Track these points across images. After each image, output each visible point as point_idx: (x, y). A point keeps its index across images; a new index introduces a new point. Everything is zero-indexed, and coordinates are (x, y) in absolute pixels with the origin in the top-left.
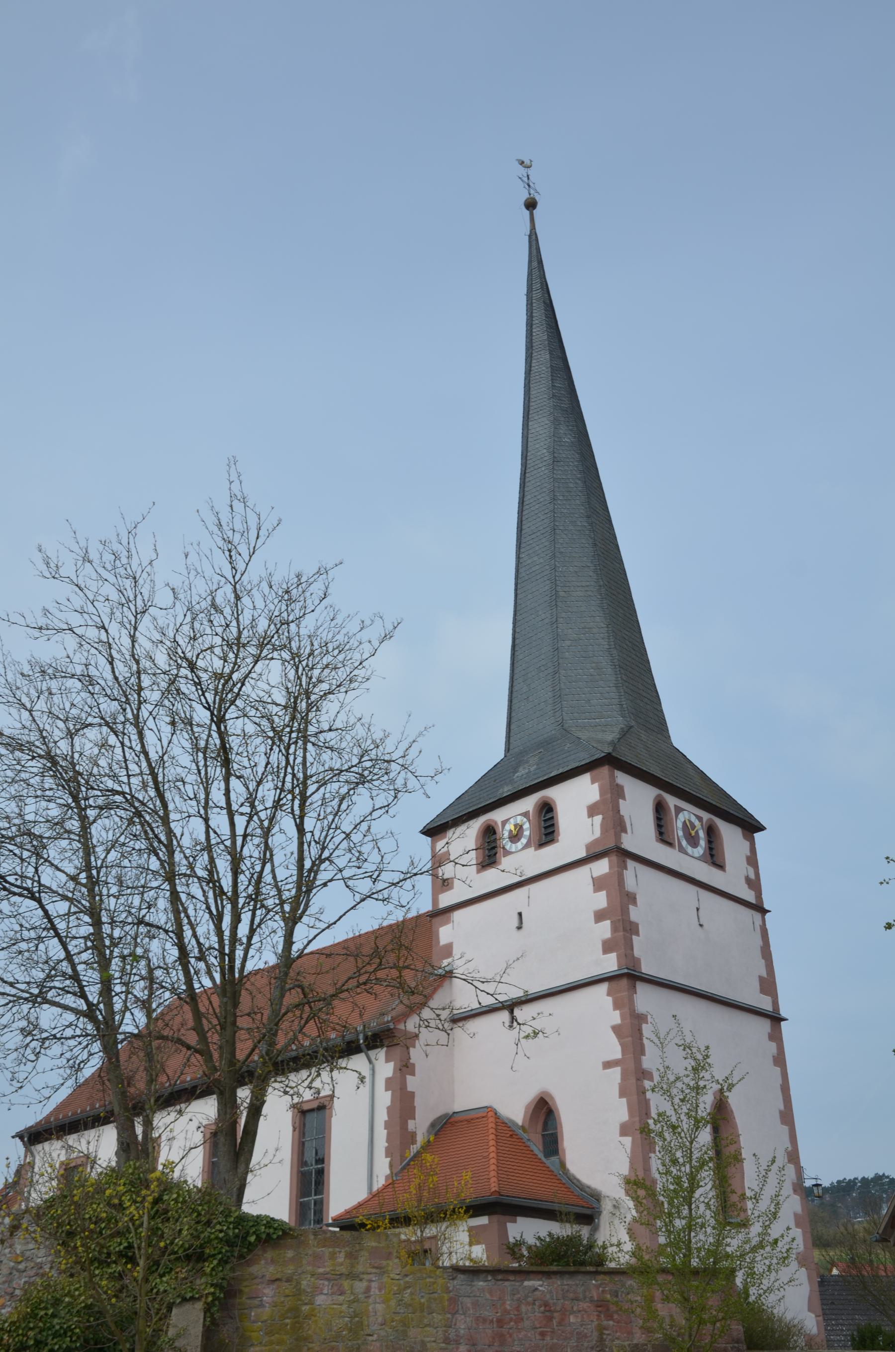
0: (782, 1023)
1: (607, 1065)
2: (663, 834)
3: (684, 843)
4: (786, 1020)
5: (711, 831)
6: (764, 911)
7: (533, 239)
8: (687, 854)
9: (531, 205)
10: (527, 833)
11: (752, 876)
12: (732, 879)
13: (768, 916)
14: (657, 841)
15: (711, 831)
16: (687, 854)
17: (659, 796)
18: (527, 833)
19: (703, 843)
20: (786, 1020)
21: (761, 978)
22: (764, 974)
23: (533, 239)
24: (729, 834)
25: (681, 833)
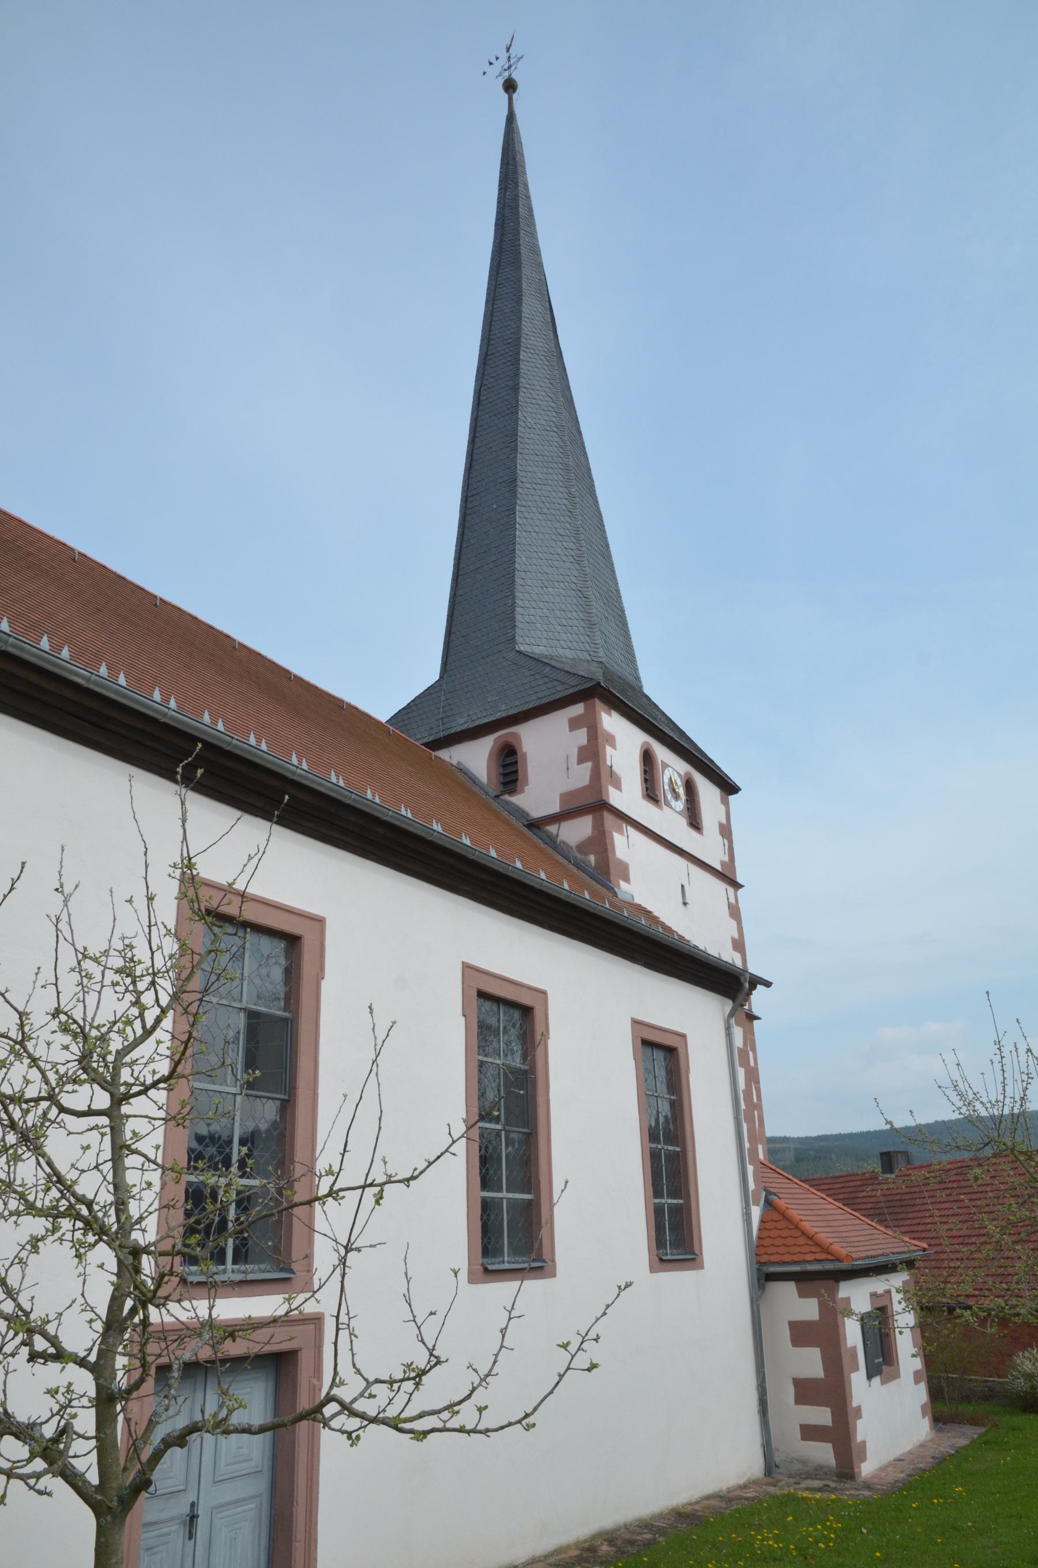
0: (755, 1022)
1: (913, 1356)
2: (651, 793)
3: (669, 796)
4: (758, 1018)
5: (690, 787)
6: (736, 885)
7: (511, 118)
8: (671, 808)
9: (510, 86)
10: (579, 856)
11: (732, 900)
12: (708, 846)
13: (740, 892)
14: (643, 797)
15: (690, 787)
16: (671, 808)
17: (646, 743)
18: (579, 856)
19: (683, 797)
20: (758, 1018)
21: (733, 940)
22: (736, 936)
23: (511, 118)
24: (707, 792)
25: (666, 787)
